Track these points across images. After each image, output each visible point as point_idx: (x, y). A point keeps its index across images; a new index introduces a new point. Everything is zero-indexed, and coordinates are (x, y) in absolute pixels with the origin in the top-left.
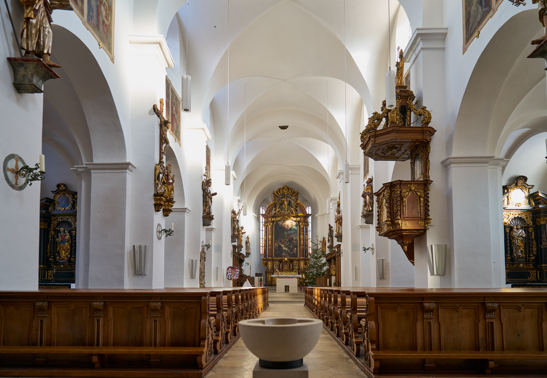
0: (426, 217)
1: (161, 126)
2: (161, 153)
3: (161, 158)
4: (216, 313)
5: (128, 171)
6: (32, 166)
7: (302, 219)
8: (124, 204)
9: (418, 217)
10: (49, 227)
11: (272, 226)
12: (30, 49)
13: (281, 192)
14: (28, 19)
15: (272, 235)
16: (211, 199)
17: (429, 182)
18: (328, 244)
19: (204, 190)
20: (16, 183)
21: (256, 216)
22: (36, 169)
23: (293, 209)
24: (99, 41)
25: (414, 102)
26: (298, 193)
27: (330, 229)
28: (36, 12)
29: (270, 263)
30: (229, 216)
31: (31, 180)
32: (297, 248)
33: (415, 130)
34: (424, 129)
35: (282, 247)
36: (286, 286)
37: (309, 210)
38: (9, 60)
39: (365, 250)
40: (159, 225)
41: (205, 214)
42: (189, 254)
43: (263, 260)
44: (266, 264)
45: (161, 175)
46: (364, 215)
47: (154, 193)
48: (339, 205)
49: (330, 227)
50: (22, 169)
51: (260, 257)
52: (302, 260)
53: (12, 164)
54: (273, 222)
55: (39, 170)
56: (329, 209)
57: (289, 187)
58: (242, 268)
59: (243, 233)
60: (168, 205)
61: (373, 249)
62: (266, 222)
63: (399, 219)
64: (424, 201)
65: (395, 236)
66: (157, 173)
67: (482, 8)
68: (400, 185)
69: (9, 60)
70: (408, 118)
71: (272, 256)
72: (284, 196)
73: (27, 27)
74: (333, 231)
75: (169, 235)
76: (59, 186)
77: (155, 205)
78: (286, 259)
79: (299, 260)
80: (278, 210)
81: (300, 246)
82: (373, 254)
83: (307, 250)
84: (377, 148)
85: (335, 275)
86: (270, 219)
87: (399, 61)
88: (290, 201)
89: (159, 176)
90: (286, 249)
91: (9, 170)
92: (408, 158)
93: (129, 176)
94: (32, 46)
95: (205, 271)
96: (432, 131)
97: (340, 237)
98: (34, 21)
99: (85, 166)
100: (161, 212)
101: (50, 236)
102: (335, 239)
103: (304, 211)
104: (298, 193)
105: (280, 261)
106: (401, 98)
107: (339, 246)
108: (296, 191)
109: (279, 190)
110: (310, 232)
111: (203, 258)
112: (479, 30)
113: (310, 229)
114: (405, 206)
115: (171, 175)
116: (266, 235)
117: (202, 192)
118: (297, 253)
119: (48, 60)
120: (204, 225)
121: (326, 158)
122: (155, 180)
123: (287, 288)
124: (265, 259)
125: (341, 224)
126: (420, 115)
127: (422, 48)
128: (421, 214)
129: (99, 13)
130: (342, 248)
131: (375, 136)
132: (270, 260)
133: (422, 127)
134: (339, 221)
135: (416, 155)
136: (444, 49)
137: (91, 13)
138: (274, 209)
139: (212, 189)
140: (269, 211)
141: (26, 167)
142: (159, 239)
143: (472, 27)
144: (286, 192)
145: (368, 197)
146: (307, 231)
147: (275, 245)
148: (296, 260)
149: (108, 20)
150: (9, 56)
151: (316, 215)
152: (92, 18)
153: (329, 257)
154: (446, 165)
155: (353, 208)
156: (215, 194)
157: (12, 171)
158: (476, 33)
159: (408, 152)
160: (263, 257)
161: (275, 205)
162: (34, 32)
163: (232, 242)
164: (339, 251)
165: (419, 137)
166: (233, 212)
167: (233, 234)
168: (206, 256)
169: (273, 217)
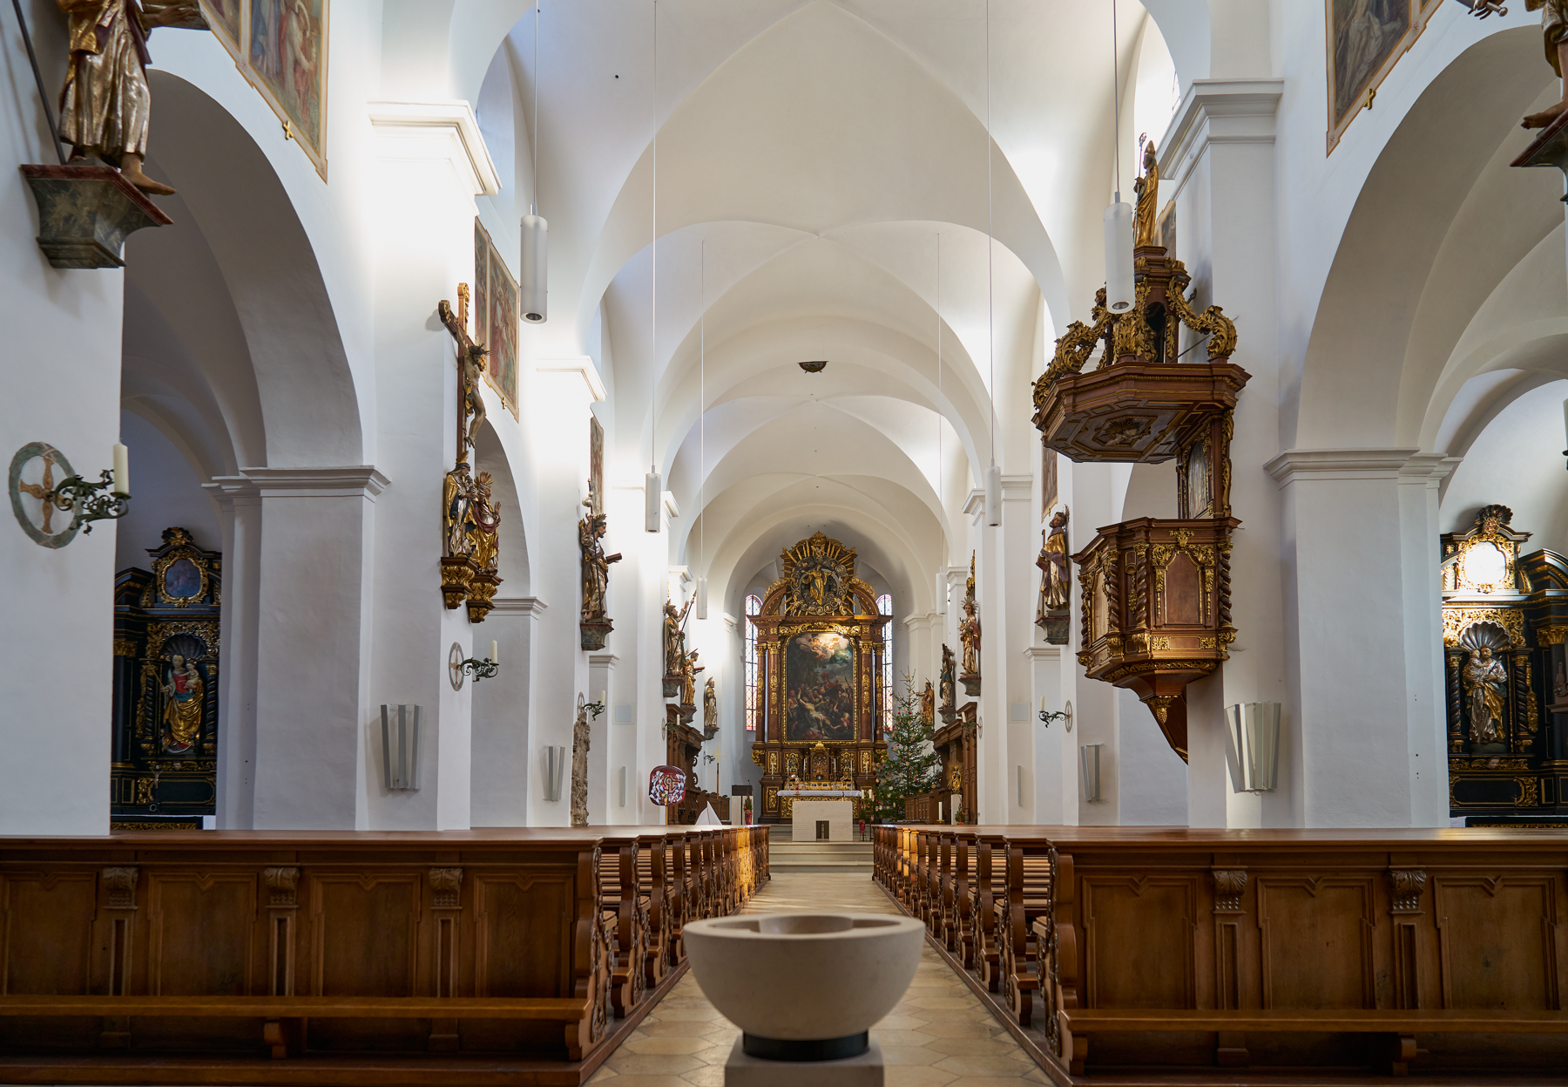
0: (1221, 624)
1: (461, 361)
2: (461, 440)
3: (461, 455)
4: (619, 899)
5: (366, 491)
6: (92, 477)
7: (867, 629)
8: (356, 585)
9: (1199, 625)
10: (141, 652)
11: (781, 650)
12: (86, 141)
13: (807, 553)
14: (80, 56)
15: (780, 676)
16: (605, 571)
17: (1230, 523)
18: (939, 702)
19: (584, 547)
20: (47, 527)
21: (734, 620)
22: (103, 486)
23: (839, 601)
24: (285, 117)
25: (1186, 294)
26: (854, 556)
27: (946, 660)
28: (103, 33)
29: (773, 758)
30: (656, 620)
31: (89, 518)
32: (851, 713)
33: (1188, 375)
34: (1216, 370)
35: (808, 711)
36: (819, 824)
37: (885, 605)
38: (27, 172)
39: (1046, 718)
40: (456, 647)
41: (588, 616)
42: (542, 731)
43: (755, 747)
44: (763, 760)
45: (462, 504)
46: (1043, 618)
47: (440, 555)
48: (971, 590)
49: (947, 653)
50: (63, 485)
51: (745, 738)
52: (865, 747)
53: (33, 472)
54: (783, 638)
55: (111, 488)
56: (944, 601)
57: (829, 537)
58: (695, 770)
59: (695, 671)
60: (482, 590)
61: (1068, 716)
62: (761, 639)
63: (1143, 631)
64: (1216, 578)
65: (1131, 679)
66: (450, 498)
67: (1382, 23)
68: (1147, 533)
69: (27, 172)
70: (1170, 338)
71: (779, 738)
72: (813, 563)
73: (78, 78)
74: (954, 664)
75: (485, 675)
76: (168, 534)
77: (445, 589)
78: (820, 744)
79: (857, 748)
80: (796, 604)
81: (860, 708)
82: (1069, 730)
83: (879, 719)
84: (1080, 426)
85: (961, 791)
86: (773, 631)
87: (1143, 176)
88: (830, 578)
89: (455, 507)
90: (820, 716)
91: (25, 488)
92: (1170, 455)
93: (371, 507)
94: (93, 132)
95: (589, 779)
96: (1239, 378)
97: (973, 681)
98: (98, 61)
99: (242, 476)
100: (462, 610)
101: (143, 679)
102: (961, 688)
103: (871, 607)
104: (854, 556)
105: (804, 751)
106: (1149, 283)
107: (971, 709)
108: (848, 548)
109: (800, 546)
110: (889, 668)
111: (582, 742)
112: (1372, 85)
113: (889, 660)
114: (1162, 593)
115: (491, 502)
116: (762, 677)
117: (578, 553)
118: (851, 727)
119: (138, 173)
120: (585, 647)
121: (933, 454)
122: (445, 518)
123: (822, 829)
124: (760, 745)
125: (976, 643)
126: (1205, 330)
127: (1209, 139)
128: (1205, 616)
129: (282, 37)
130: (980, 712)
131: (1076, 392)
132: (773, 747)
133: (1210, 367)
134: (972, 634)
135: (1193, 445)
136: (1272, 140)
137: (261, 38)
138: (785, 600)
139: (609, 544)
140: (770, 606)
141: (75, 481)
142: (457, 686)
143: (1353, 76)
144: (819, 551)
145: (1054, 567)
146: (879, 665)
147: (789, 704)
148: (850, 748)
149: (308, 58)
150: (26, 162)
151: (906, 620)
152: (263, 52)
153: (944, 738)
154: (1278, 474)
155: (1013, 597)
156: (617, 558)
157: (35, 491)
158: (1365, 96)
160: (753, 739)
161: (789, 589)
162: (97, 91)
163: (665, 695)
164: (973, 721)
165: (1201, 393)
166: (669, 610)
167: (669, 673)
168: (591, 737)
169: (784, 623)
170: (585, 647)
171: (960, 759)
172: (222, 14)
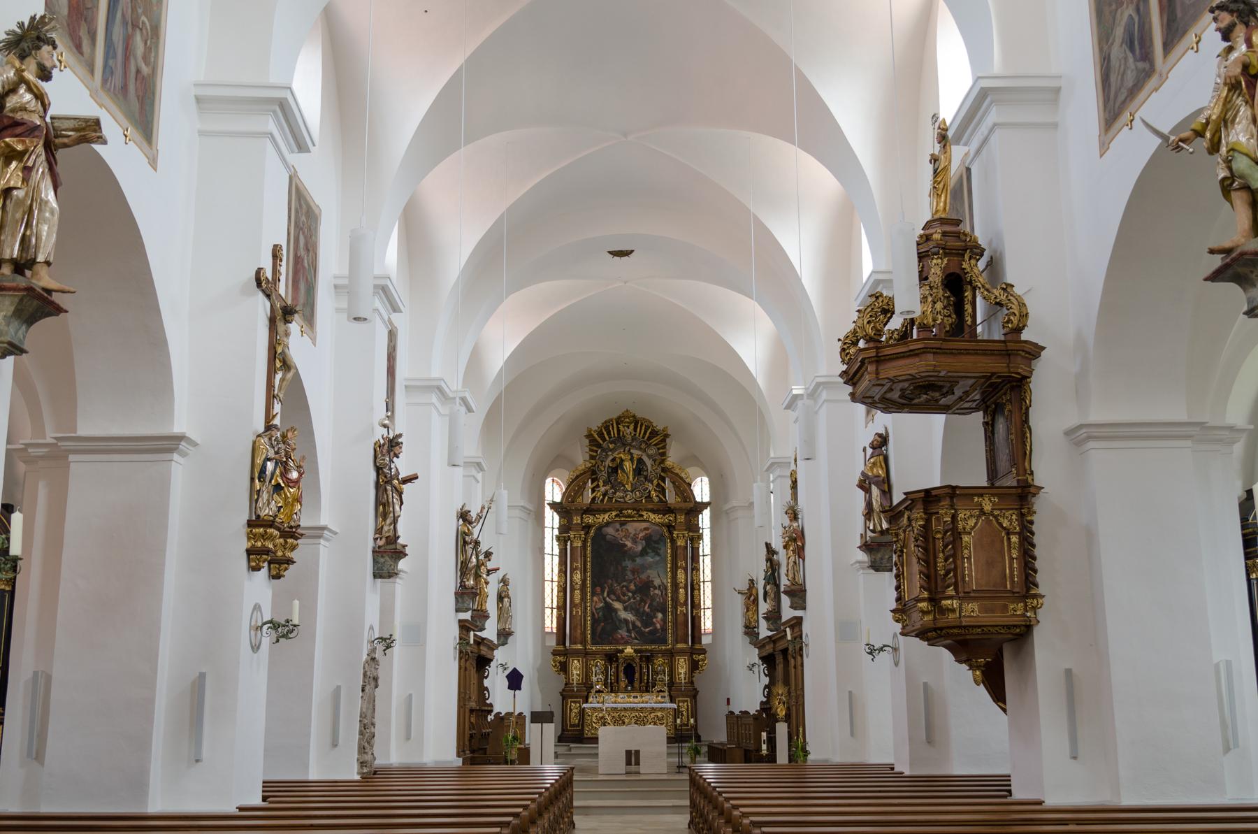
0: (1028, 589)
1: (272, 321)
2: (271, 397)
3: (269, 416)
5: (176, 456)
7: (681, 518)
9: (1006, 592)
11: (585, 542)
13: (614, 432)
15: (584, 571)
16: (400, 494)
17: (1032, 490)
18: (764, 607)
19: (378, 470)
23: (650, 487)
24: (126, 123)
25: (982, 264)
26: (667, 436)
27: (769, 560)
28: (27, 170)
29: (576, 668)
32: (664, 612)
34: (1011, 346)
35: (616, 611)
36: (628, 753)
37: (701, 489)
40: (257, 608)
41: (380, 543)
42: (327, 664)
43: (555, 653)
44: (564, 668)
45: (270, 466)
47: (247, 518)
49: (770, 551)
52: (682, 652)
54: (587, 528)
57: (639, 415)
58: (486, 683)
59: (489, 572)
60: (284, 546)
61: (895, 650)
62: (564, 529)
63: (951, 598)
65: (948, 642)
66: (259, 461)
67: (1136, 60)
70: (968, 307)
71: (584, 642)
72: (620, 441)
74: (779, 565)
75: (285, 636)
77: (249, 552)
78: (629, 650)
79: (671, 655)
80: (602, 489)
81: (675, 607)
82: (896, 664)
84: (885, 388)
85: (788, 718)
86: (577, 520)
88: (640, 461)
89: (263, 470)
90: (629, 616)
92: (976, 409)
93: (179, 469)
95: (376, 720)
96: (1034, 351)
97: (798, 594)
99: (49, 440)
102: (785, 601)
103: (684, 489)
104: (667, 436)
105: (611, 658)
106: (946, 255)
107: (797, 623)
108: (660, 427)
109: (607, 426)
110: (708, 560)
111: (371, 681)
112: (1132, 107)
113: (707, 550)
114: (969, 558)
116: (563, 571)
117: (372, 475)
118: (664, 629)
119: (43, 279)
120: (377, 575)
121: (752, 343)
122: (252, 479)
123: (632, 758)
124: (562, 651)
125: (800, 552)
126: (999, 304)
127: (995, 125)
130: (806, 627)
131: (879, 360)
132: (576, 653)
133: (1004, 342)
134: (796, 541)
135: (997, 405)
136: (1055, 126)
137: (111, 62)
139: (402, 465)
140: (574, 489)
142: (256, 648)
144: (628, 431)
145: (875, 491)
147: (594, 603)
148: (664, 653)
149: (147, 64)
151: (727, 507)
152: (112, 73)
153: (769, 649)
155: (837, 524)
156: (411, 479)
158: (1126, 116)
160: (552, 643)
161: (594, 472)
164: (799, 637)
165: (998, 366)
166: (464, 516)
167: (463, 585)
168: (381, 673)
169: (589, 511)
170: (377, 575)
171: (786, 682)
172: (82, 53)
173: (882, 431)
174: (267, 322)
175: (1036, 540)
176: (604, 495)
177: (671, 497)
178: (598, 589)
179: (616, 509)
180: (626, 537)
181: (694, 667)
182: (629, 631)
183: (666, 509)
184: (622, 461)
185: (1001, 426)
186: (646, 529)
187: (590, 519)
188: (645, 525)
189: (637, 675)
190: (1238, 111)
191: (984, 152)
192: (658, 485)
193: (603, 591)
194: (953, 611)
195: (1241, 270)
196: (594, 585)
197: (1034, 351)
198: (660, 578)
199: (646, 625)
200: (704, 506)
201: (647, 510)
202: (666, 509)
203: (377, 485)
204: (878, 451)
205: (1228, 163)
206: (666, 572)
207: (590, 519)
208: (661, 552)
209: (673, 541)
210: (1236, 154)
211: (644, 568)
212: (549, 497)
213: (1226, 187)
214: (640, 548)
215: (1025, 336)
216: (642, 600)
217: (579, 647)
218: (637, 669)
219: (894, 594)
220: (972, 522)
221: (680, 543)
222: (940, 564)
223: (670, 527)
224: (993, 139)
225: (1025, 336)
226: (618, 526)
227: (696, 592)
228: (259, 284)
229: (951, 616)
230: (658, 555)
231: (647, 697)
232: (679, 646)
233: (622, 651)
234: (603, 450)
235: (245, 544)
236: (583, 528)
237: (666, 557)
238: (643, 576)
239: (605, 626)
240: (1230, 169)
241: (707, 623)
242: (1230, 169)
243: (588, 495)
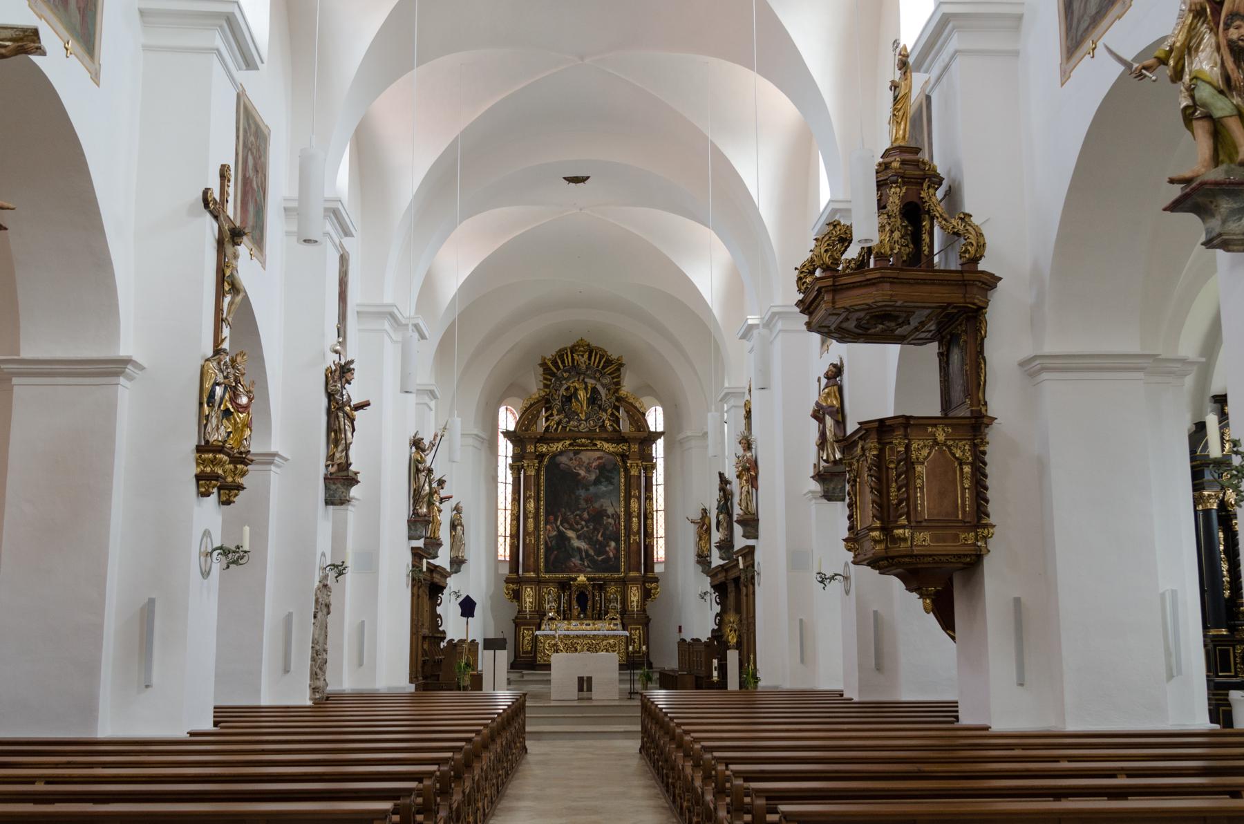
0: (980, 519)
1: (220, 243)
2: (219, 321)
3: (217, 341)
5: (122, 380)
7: (635, 448)
8: (109, 475)
9: (958, 521)
11: (538, 471)
15: (538, 500)
16: (352, 420)
17: (986, 421)
18: (716, 536)
19: (330, 396)
25: (940, 194)
26: (621, 365)
27: (722, 489)
29: (529, 595)
30: (405, 452)
32: (617, 541)
34: (967, 276)
35: (569, 539)
36: (581, 679)
37: (655, 419)
39: (823, 580)
40: (207, 533)
41: (332, 470)
42: (279, 591)
43: (508, 581)
44: (517, 596)
45: (219, 391)
47: (194, 442)
48: (749, 413)
49: (724, 481)
51: (496, 569)
54: (541, 457)
57: (593, 344)
58: (439, 610)
60: (234, 472)
61: (846, 578)
63: (903, 527)
64: (973, 474)
65: (899, 570)
66: (208, 386)
68: (906, 431)
70: (926, 237)
71: (537, 570)
72: (575, 369)
74: (732, 494)
75: (235, 562)
77: (198, 478)
78: (582, 578)
79: (624, 583)
80: (556, 418)
81: (628, 536)
82: (847, 592)
83: (649, 550)
84: (841, 318)
86: (530, 448)
87: (897, 79)
88: (594, 390)
90: (582, 545)
92: (932, 340)
93: (126, 392)
96: (991, 282)
97: (751, 524)
100: (214, 498)
102: (738, 530)
103: (638, 419)
104: (621, 365)
105: (564, 586)
106: (904, 183)
107: (749, 552)
109: (561, 354)
110: (661, 489)
111: (323, 607)
112: (1094, 35)
113: (661, 480)
114: (922, 488)
116: (516, 499)
117: (324, 401)
118: (617, 557)
120: (328, 502)
121: (708, 272)
122: (201, 404)
123: (585, 684)
124: (515, 580)
125: (753, 481)
126: (957, 234)
127: (956, 52)
131: (836, 289)
133: (961, 272)
134: (749, 471)
135: (952, 335)
136: (1016, 53)
139: (354, 392)
140: (528, 418)
142: (206, 574)
143: (1079, 22)
144: (582, 360)
145: (829, 421)
147: (547, 532)
148: (616, 581)
151: (681, 436)
158: (1088, 44)
159: (932, 326)
160: (505, 570)
161: (548, 401)
163: (410, 538)
164: (750, 566)
165: (954, 296)
167: (415, 513)
168: (333, 601)
169: (544, 439)
170: (328, 502)
173: (837, 361)
174: (215, 244)
175: (988, 470)
176: (558, 424)
177: (625, 426)
178: (551, 517)
179: (570, 438)
180: (580, 466)
181: (646, 595)
182: (581, 559)
183: (619, 438)
184: (576, 390)
185: (956, 357)
186: (599, 458)
187: (544, 448)
188: (598, 454)
189: (590, 603)
190: (1202, 39)
191: (945, 79)
192: (612, 414)
193: (556, 520)
194: (905, 540)
195: (1200, 200)
196: (547, 514)
197: (991, 282)
198: (613, 507)
199: (599, 553)
200: (655, 436)
201: (601, 439)
202: (619, 438)
203: (329, 412)
204: (832, 381)
205: (1191, 91)
206: (619, 501)
207: (544, 448)
208: (615, 481)
209: (627, 470)
210: (1199, 83)
211: (597, 497)
212: (502, 426)
213: (1188, 116)
214: (593, 477)
215: (982, 266)
216: (595, 529)
217: (532, 575)
218: (590, 596)
219: (847, 523)
220: (925, 452)
221: (634, 472)
222: (893, 494)
223: (624, 457)
224: (954, 66)
225: (982, 266)
226: (571, 455)
227: (649, 521)
228: (206, 205)
229: (903, 545)
230: (612, 483)
231: (599, 624)
232: (632, 574)
233: (575, 579)
234: (558, 379)
235: (194, 470)
236: (537, 457)
237: (619, 485)
238: (597, 505)
239: (558, 554)
240: (1192, 97)
241: (660, 552)
242: (1192, 97)
243: (542, 424)
